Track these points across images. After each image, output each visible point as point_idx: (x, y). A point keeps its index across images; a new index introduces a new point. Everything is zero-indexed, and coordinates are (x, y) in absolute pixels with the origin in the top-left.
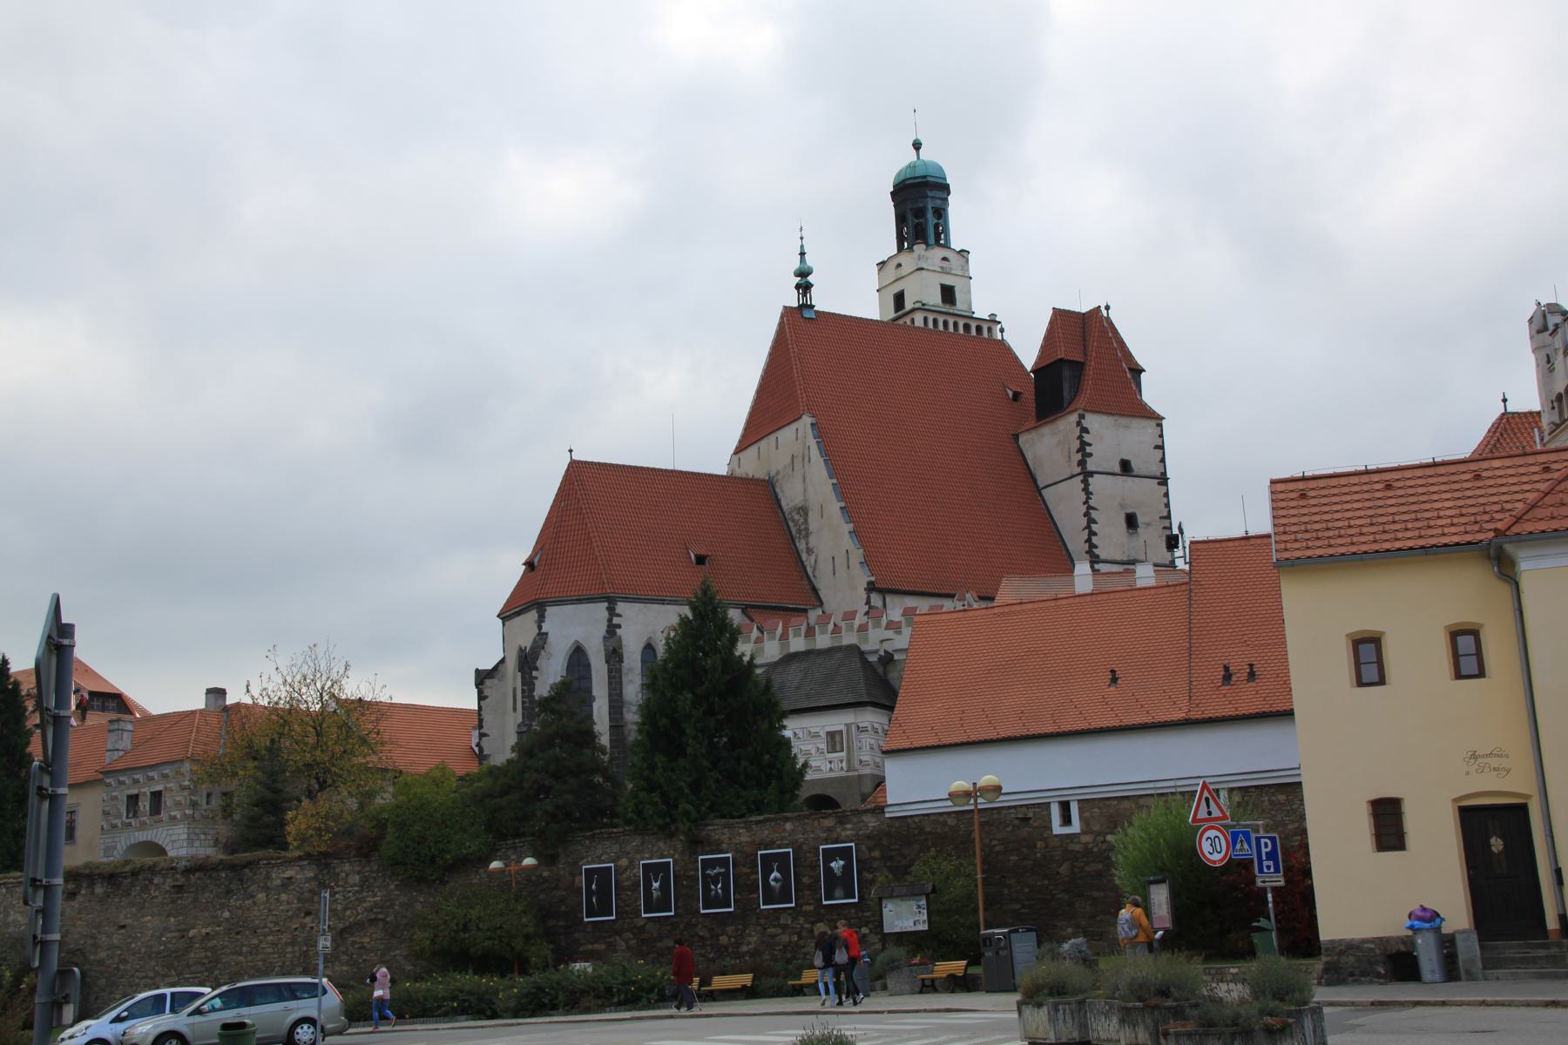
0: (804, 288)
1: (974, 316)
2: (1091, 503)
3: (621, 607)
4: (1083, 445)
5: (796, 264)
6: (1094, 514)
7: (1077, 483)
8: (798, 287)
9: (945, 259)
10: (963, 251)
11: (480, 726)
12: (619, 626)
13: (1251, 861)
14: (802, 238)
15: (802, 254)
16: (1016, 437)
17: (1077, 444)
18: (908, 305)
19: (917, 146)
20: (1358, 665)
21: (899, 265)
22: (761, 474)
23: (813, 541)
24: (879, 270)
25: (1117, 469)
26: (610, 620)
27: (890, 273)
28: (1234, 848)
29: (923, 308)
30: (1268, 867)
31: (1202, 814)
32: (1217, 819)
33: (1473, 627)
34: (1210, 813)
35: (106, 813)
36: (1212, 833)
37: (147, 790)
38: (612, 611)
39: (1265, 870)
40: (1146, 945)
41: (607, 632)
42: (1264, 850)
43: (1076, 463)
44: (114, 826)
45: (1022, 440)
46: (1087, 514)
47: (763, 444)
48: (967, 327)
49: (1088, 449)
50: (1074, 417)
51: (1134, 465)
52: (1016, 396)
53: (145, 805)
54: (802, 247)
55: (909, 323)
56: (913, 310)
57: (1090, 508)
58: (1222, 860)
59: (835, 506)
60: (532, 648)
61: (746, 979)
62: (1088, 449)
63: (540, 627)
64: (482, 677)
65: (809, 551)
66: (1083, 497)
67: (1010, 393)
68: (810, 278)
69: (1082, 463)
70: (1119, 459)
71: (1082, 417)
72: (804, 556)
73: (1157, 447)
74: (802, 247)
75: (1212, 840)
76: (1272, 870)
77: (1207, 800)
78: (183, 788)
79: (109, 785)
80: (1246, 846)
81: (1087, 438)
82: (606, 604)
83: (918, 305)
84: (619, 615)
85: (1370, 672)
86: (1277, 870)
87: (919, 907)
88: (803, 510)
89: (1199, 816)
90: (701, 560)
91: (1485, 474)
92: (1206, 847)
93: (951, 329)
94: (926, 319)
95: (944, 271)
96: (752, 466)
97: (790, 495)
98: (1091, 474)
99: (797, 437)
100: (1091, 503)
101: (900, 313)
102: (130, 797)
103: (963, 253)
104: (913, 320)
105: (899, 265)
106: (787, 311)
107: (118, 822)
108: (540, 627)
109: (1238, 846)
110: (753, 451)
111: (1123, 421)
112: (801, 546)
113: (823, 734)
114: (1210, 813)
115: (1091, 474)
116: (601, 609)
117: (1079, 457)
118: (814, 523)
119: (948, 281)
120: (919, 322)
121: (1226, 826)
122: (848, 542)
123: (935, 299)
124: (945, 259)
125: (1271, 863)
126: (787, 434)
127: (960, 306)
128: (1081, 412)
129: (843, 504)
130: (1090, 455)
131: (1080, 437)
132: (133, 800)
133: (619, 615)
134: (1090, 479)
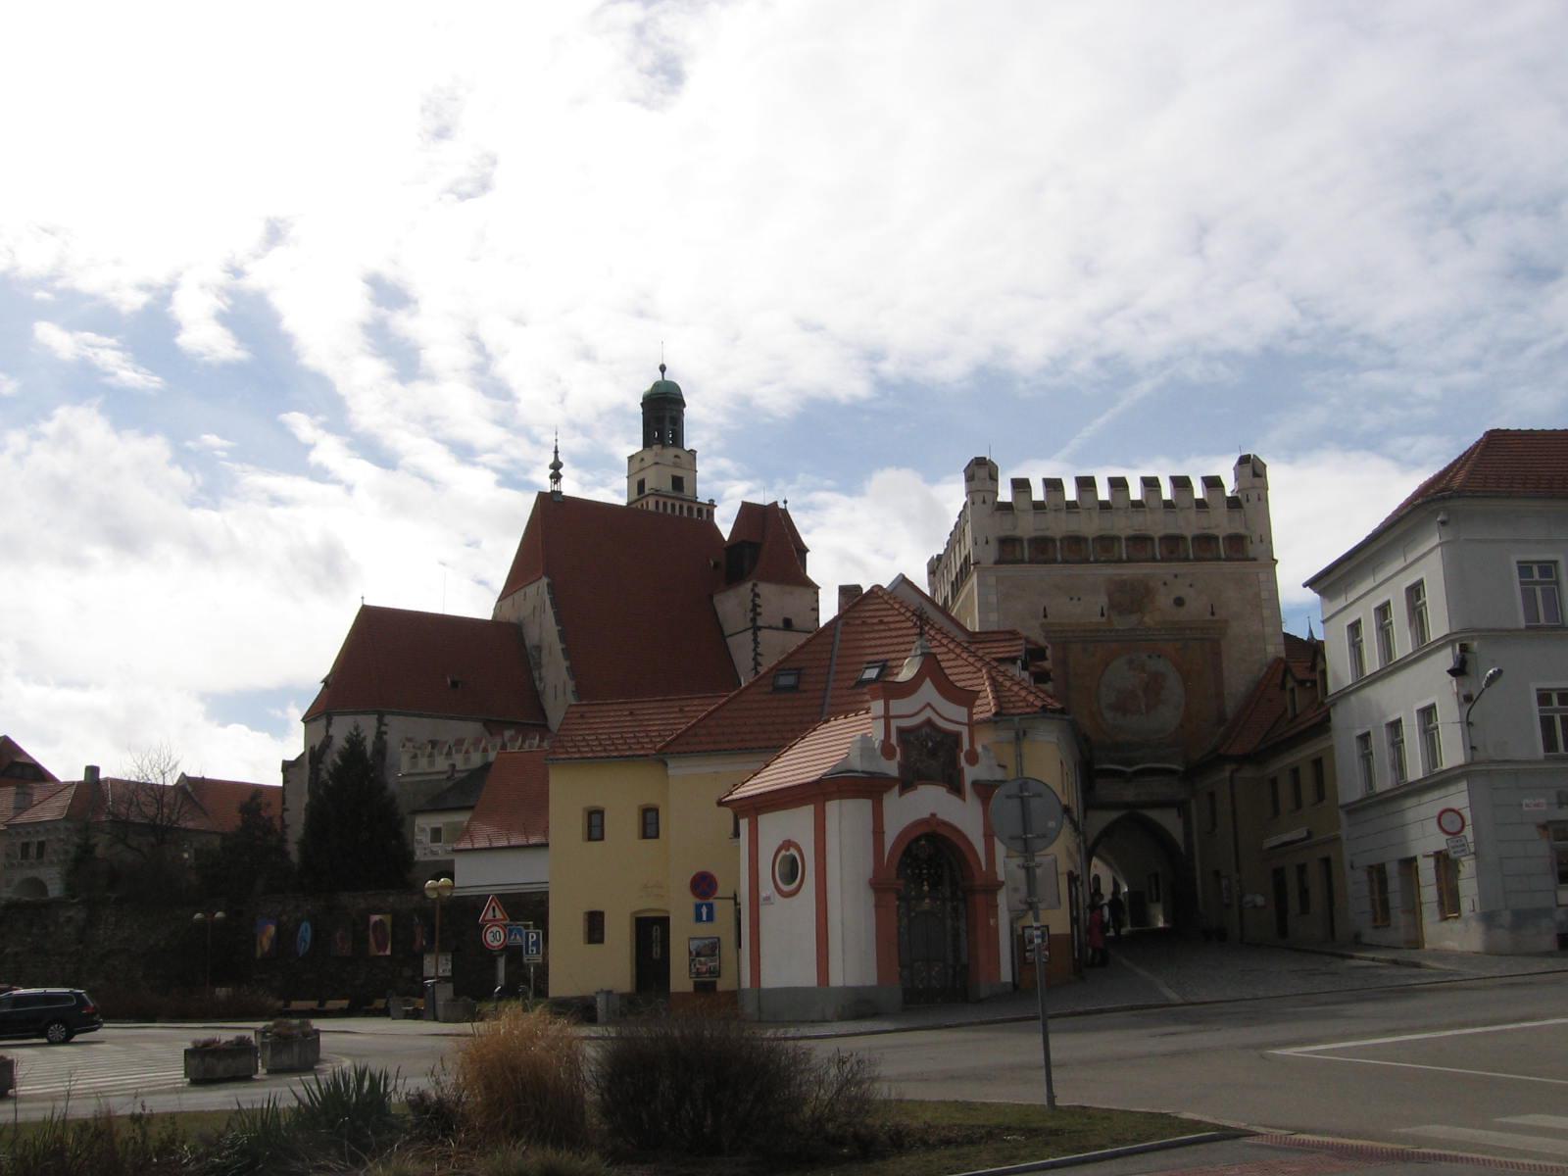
0: (556, 477)
1: (698, 500)
2: (759, 650)
3: (388, 719)
4: (755, 606)
5: (551, 460)
6: (759, 658)
7: (749, 634)
8: (551, 477)
9: (676, 456)
10: (692, 450)
11: (284, 803)
12: (386, 733)
13: (522, 946)
15: (556, 452)
16: (711, 597)
17: (750, 606)
18: (647, 491)
20: (590, 826)
21: (642, 460)
22: (513, 620)
23: (544, 672)
24: (629, 461)
25: (781, 625)
26: (379, 728)
28: (510, 937)
29: (656, 493)
30: (532, 951)
31: (490, 916)
33: (641, 813)
34: (494, 917)
35: (8, 855)
36: (495, 929)
37: (35, 840)
38: (381, 722)
40: (735, 987)
41: (376, 737)
43: (749, 619)
44: (12, 865)
45: (716, 598)
46: (754, 659)
48: (690, 509)
49: (759, 610)
50: (749, 585)
51: (794, 622)
52: (716, 565)
53: (33, 851)
54: (556, 447)
55: (639, 507)
56: (649, 495)
57: (757, 654)
59: (558, 646)
60: (321, 746)
61: (345, 1003)
62: (759, 610)
63: (327, 731)
64: (287, 767)
65: (541, 679)
66: (752, 646)
67: (712, 563)
68: (561, 471)
69: (754, 620)
70: (782, 618)
71: (755, 585)
72: (537, 683)
73: (813, 609)
74: (556, 447)
75: (494, 936)
77: (494, 908)
78: (60, 840)
79: (10, 835)
80: (518, 937)
81: (758, 601)
82: (376, 716)
83: (652, 491)
84: (386, 725)
85: (596, 833)
86: (538, 953)
87: (447, 960)
88: (539, 648)
89: (486, 918)
90: (454, 684)
91: (687, 709)
92: (489, 937)
93: (669, 510)
94: (657, 503)
95: (676, 465)
96: (511, 616)
97: (532, 636)
98: (759, 628)
99: (538, 591)
100: (759, 650)
101: (642, 496)
102: (23, 844)
103: (692, 453)
104: (642, 505)
105: (642, 460)
107: (15, 862)
108: (327, 731)
109: (513, 937)
110: (509, 601)
111: (788, 588)
112: (536, 674)
113: (428, 830)
115: (759, 628)
117: (751, 615)
118: (545, 659)
119: (679, 473)
120: (652, 507)
121: (505, 926)
122: (564, 675)
123: (667, 486)
124: (676, 456)
126: (531, 590)
127: (687, 492)
128: (754, 581)
129: (564, 646)
130: (760, 614)
131: (753, 601)
132: (26, 846)
133: (386, 725)
134: (759, 633)
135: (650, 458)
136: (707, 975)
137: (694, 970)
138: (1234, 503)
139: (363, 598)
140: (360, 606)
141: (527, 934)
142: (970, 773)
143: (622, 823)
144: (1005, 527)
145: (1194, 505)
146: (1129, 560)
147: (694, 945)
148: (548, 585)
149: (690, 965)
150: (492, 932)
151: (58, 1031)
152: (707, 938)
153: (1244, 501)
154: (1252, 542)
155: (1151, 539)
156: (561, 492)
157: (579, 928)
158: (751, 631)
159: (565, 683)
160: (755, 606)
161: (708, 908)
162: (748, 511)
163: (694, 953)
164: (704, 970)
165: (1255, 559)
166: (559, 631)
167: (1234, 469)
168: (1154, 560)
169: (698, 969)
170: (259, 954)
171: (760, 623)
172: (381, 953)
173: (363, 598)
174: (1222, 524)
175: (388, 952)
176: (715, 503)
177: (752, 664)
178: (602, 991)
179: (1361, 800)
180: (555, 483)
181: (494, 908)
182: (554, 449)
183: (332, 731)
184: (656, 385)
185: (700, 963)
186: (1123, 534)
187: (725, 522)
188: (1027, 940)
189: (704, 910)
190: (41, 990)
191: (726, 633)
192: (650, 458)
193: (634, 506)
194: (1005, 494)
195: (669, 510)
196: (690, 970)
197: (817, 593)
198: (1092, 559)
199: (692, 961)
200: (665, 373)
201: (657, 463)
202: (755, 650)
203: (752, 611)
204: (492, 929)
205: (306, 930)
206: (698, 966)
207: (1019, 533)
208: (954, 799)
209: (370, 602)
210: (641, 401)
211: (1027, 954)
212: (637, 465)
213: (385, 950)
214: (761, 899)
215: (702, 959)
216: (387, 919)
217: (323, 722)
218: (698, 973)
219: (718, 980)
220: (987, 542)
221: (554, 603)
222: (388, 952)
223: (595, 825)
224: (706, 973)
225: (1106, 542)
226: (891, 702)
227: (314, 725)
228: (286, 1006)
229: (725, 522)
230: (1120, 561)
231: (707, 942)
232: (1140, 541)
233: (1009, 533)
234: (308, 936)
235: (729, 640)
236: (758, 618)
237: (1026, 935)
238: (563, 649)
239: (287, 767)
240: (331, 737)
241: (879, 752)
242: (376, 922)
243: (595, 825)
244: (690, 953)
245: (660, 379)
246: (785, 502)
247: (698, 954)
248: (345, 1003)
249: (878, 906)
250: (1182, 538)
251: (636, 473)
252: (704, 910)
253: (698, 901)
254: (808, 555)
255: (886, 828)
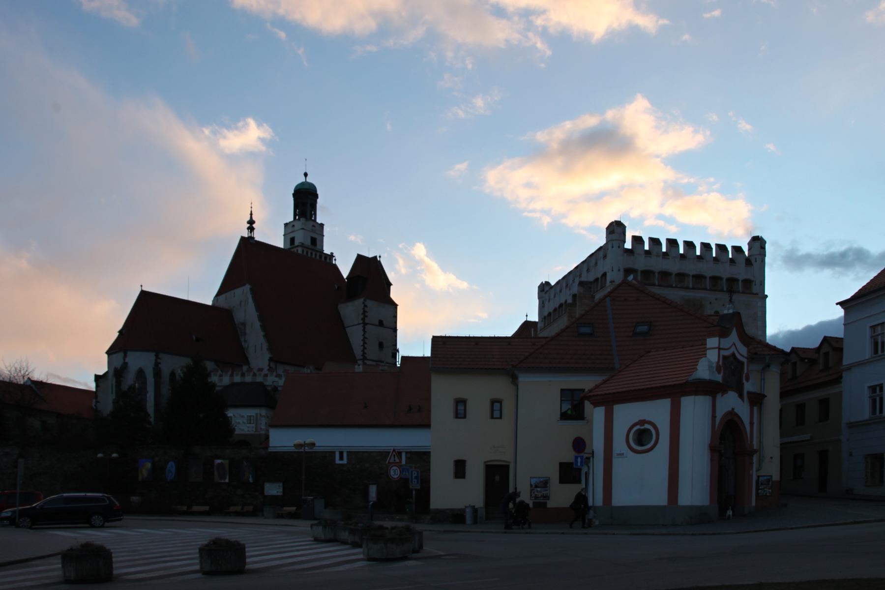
0: (251, 229)
5: (248, 219)
6: (366, 340)
7: (360, 327)
8: (248, 228)
12: (160, 363)
14: (251, 207)
15: (251, 214)
17: (362, 311)
19: (306, 175)
21: (293, 226)
24: (285, 227)
25: (377, 323)
26: (156, 360)
27: (290, 229)
29: (302, 245)
30: (415, 482)
32: (397, 463)
34: (395, 460)
36: (395, 468)
38: (157, 357)
39: (413, 482)
42: (414, 475)
47: (228, 294)
48: (320, 257)
49: (366, 314)
50: (361, 300)
54: (251, 212)
56: (298, 246)
58: (398, 478)
59: (258, 324)
61: (207, 508)
63: (124, 360)
64: (98, 378)
65: (245, 341)
66: (362, 333)
68: (254, 226)
72: (243, 343)
74: (251, 212)
75: (395, 472)
76: (416, 482)
77: (394, 456)
80: (407, 473)
84: (160, 359)
86: (418, 483)
87: (279, 486)
88: (244, 324)
90: (197, 340)
92: (392, 472)
93: (314, 256)
95: (313, 231)
96: (222, 304)
97: (239, 317)
99: (243, 292)
101: (293, 246)
105: (293, 226)
106: (243, 238)
108: (124, 360)
109: (404, 473)
110: (223, 296)
112: (242, 339)
114: (395, 460)
116: (151, 356)
117: (362, 316)
119: (315, 236)
123: (308, 242)
125: (416, 480)
126: (239, 291)
127: (318, 247)
130: (367, 316)
133: (160, 359)
134: (366, 327)
135: (298, 225)
136: (542, 498)
137: (533, 495)
138: (748, 261)
139: (141, 286)
140: (140, 290)
141: (412, 472)
142: (748, 387)
143: (478, 408)
144: (630, 263)
145: (729, 260)
146: (693, 288)
147: (533, 481)
148: (251, 289)
149: (531, 493)
150: (393, 470)
151: (97, 520)
152: (542, 478)
153: (753, 262)
154: (755, 285)
155: (705, 277)
156: (254, 238)
157: (469, 469)
158: (362, 325)
159: (262, 344)
160: (365, 312)
161: (581, 459)
162: (361, 260)
163: (534, 486)
164: (540, 495)
165: (757, 294)
166: (258, 315)
167: (748, 244)
168: (705, 289)
169: (536, 495)
170: (140, 478)
171: (367, 321)
172: (223, 481)
173: (141, 286)
174: (741, 273)
175: (227, 481)
176: (334, 255)
177: (362, 343)
178: (470, 506)
179: (866, 420)
180: (251, 232)
181: (394, 456)
182: (250, 213)
183: (127, 360)
184: (302, 184)
185: (537, 491)
186: (691, 274)
187: (345, 269)
188: (760, 483)
189: (579, 460)
190: (83, 494)
191: (346, 325)
192: (298, 225)
193: (292, 250)
194: (628, 245)
195: (314, 256)
196: (531, 495)
197: (396, 308)
198: (674, 285)
199: (532, 490)
200: (307, 178)
201: (302, 229)
202: (363, 335)
203: (363, 314)
204: (392, 468)
205: (171, 467)
206: (536, 493)
207: (636, 267)
208: (740, 400)
209: (147, 288)
210: (293, 192)
211: (760, 491)
212: (290, 229)
213: (225, 478)
214: (614, 455)
215: (539, 489)
216: (226, 463)
217: (121, 354)
218: (536, 497)
219: (548, 501)
220: (619, 270)
221: (255, 299)
222: (227, 481)
223: (460, 408)
224: (541, 497)
225: (681, 276)
226: (721, 339)
227: (114, 356)
228: (242, 509)
229: (345, 269)
230: (688, 288)
231: (542, 480)
232: (699, 277)
233: (631, 266)
234: (174, 470)
235: (348, 330)
236: (366, 318)
237: (760, 480)
238: (261, 325)
239: (98, 378)
240: (127, 363)
241: (715, 370)
242: (218, 464)
243: (460, 408)
244: (531, 485)
245: (304, 181)
246: (380, 257)
247: (536, 486)
248: (207, 508)
249: (712, 460)
250: (721, 278)
251: (289, 233)
252: (579, 460)
253: (577, 454)
254: (392, 287)
255: (717, 414)
